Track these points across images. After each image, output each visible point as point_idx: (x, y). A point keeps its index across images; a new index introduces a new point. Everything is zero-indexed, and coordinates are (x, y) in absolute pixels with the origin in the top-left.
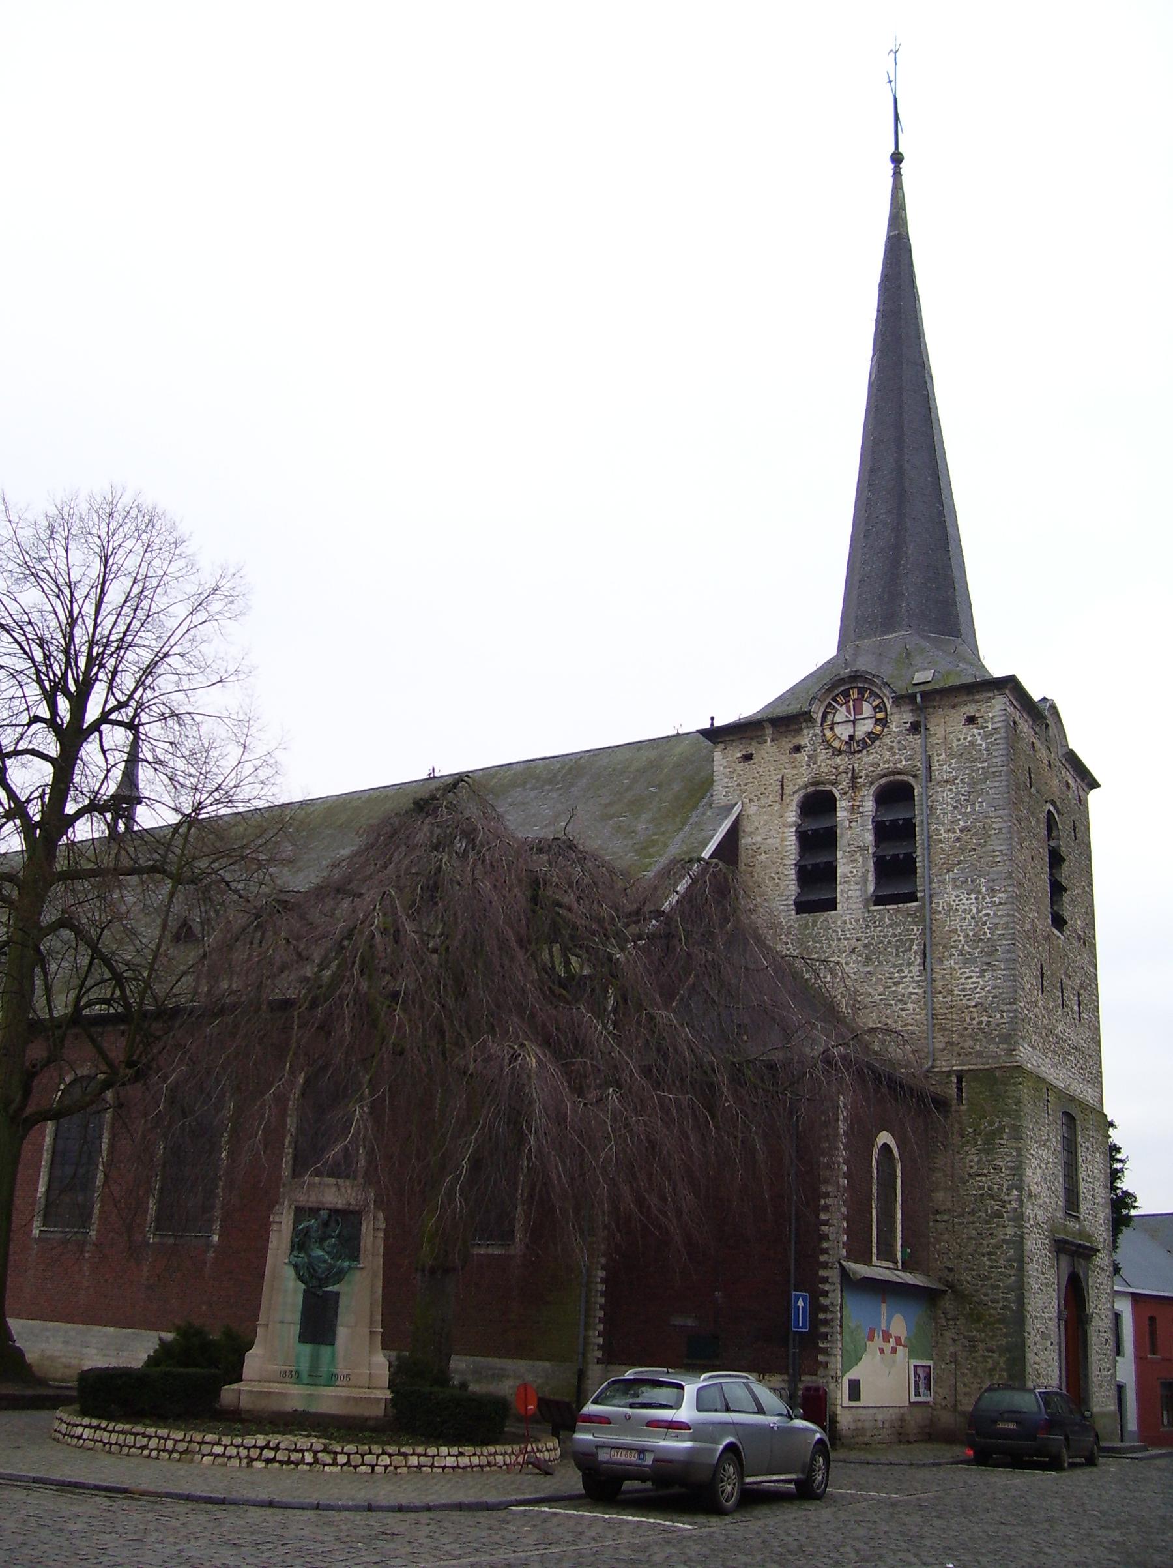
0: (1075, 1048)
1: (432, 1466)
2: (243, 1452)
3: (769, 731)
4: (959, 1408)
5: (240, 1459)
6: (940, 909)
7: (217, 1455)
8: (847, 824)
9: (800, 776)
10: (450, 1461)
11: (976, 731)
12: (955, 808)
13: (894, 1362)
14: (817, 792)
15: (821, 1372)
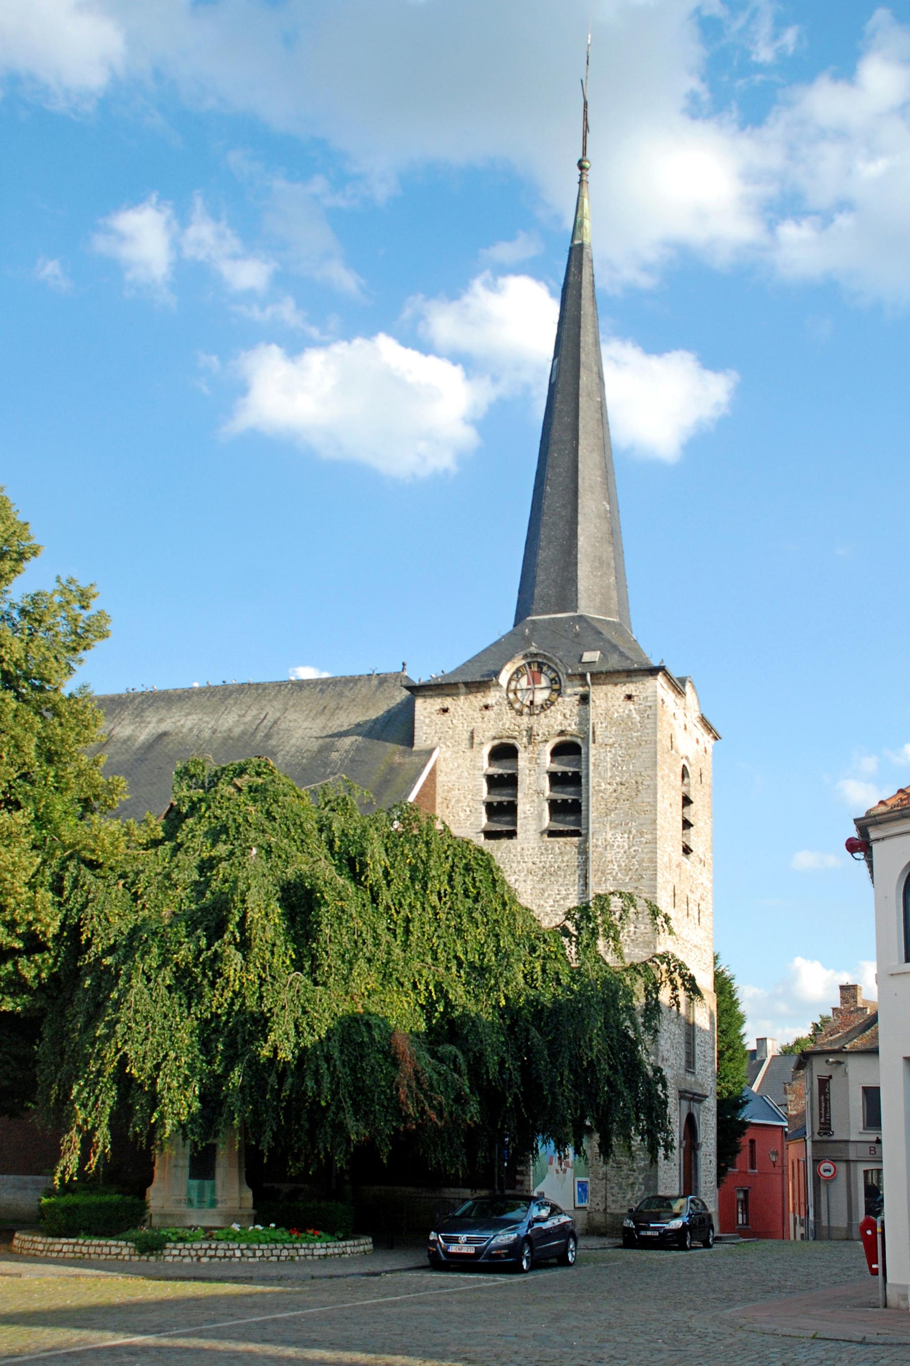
0: (695, 946)
1: (313, 1255)
2: (193, 1253)
3: (463, 689)
4: (608, 1211)
5: (192, 1258)
6: (600, 843)
7: (175, 1256)
8: (527, 772)
9: (489, 734)
10: (322, 1252)
11: (632, 707)
12: (614, 766)
13: (565, 1178)
14: (502, 744)
15: (518, 1187)
